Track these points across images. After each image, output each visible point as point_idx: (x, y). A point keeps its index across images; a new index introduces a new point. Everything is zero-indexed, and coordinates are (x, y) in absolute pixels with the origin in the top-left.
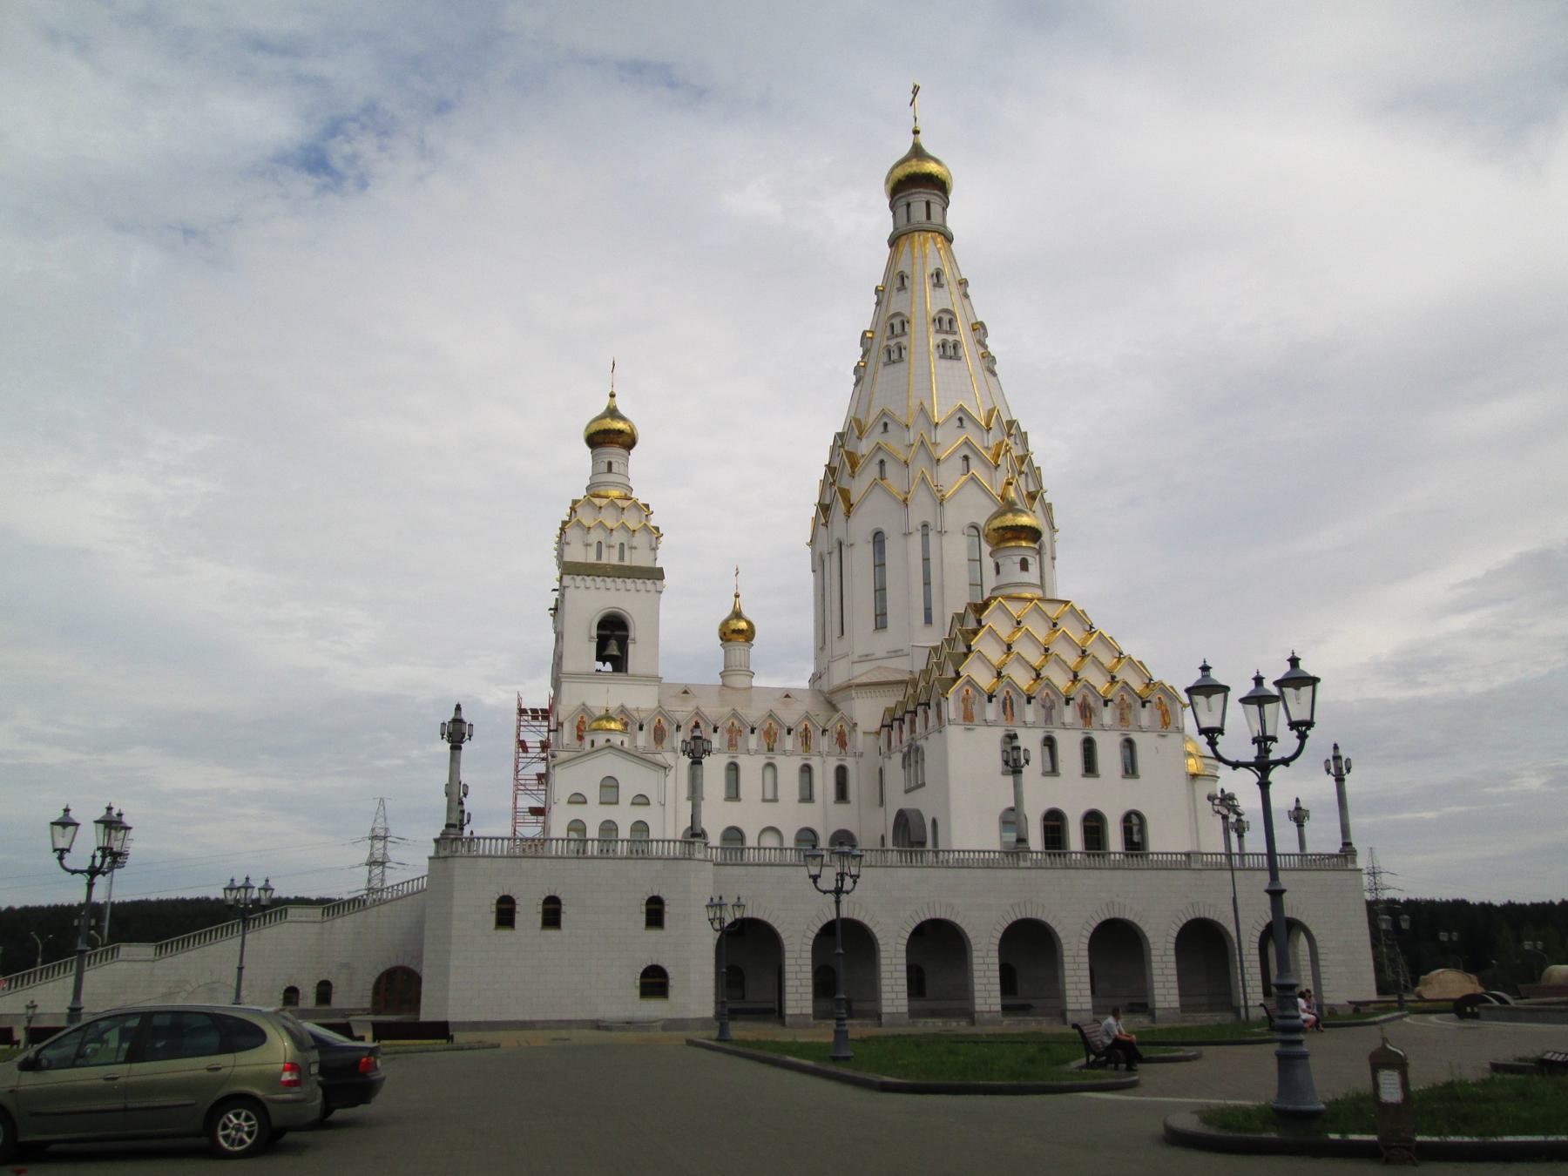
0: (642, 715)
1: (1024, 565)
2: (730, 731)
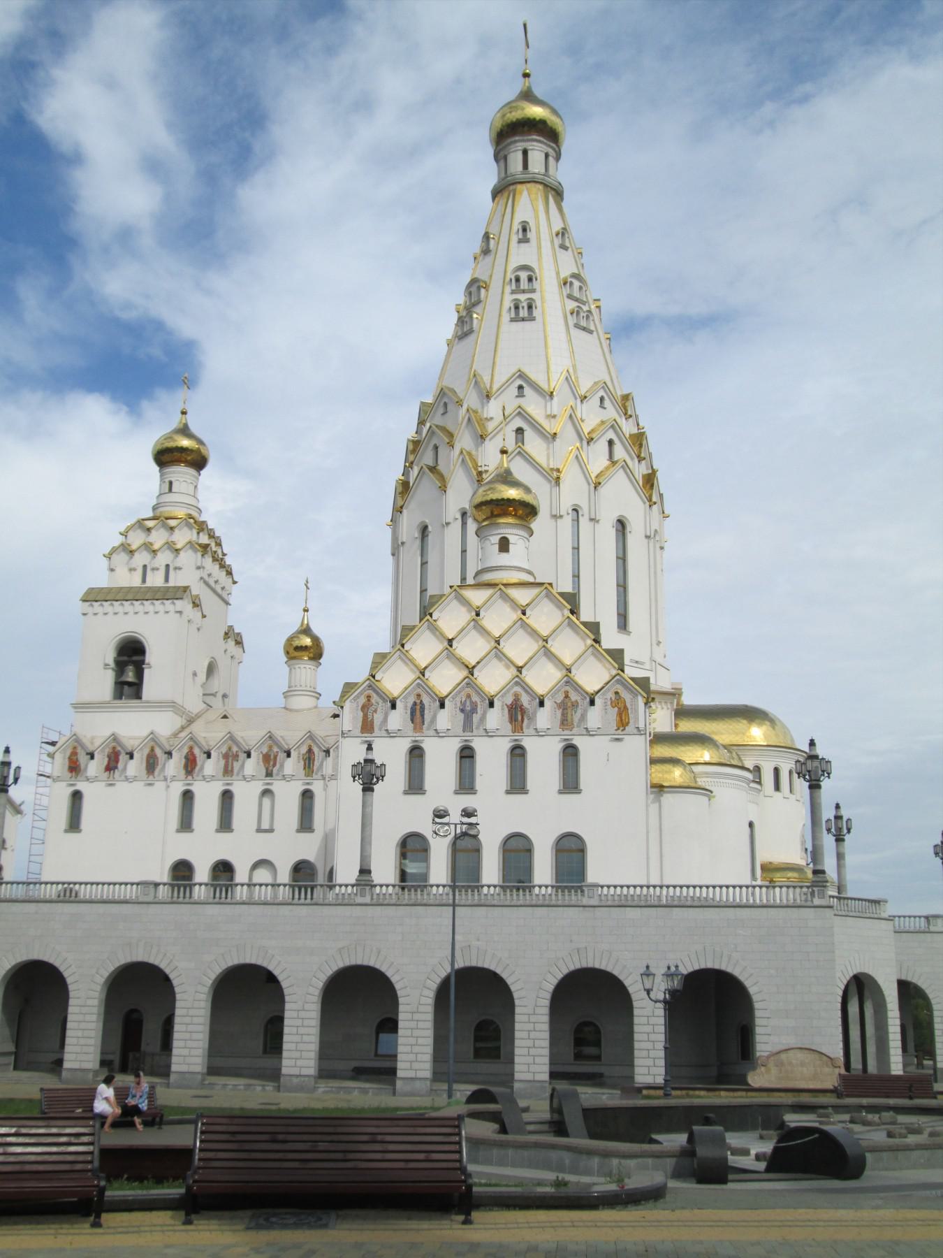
0: (132, 742)
1: (504, 545)
2: (226, 756)
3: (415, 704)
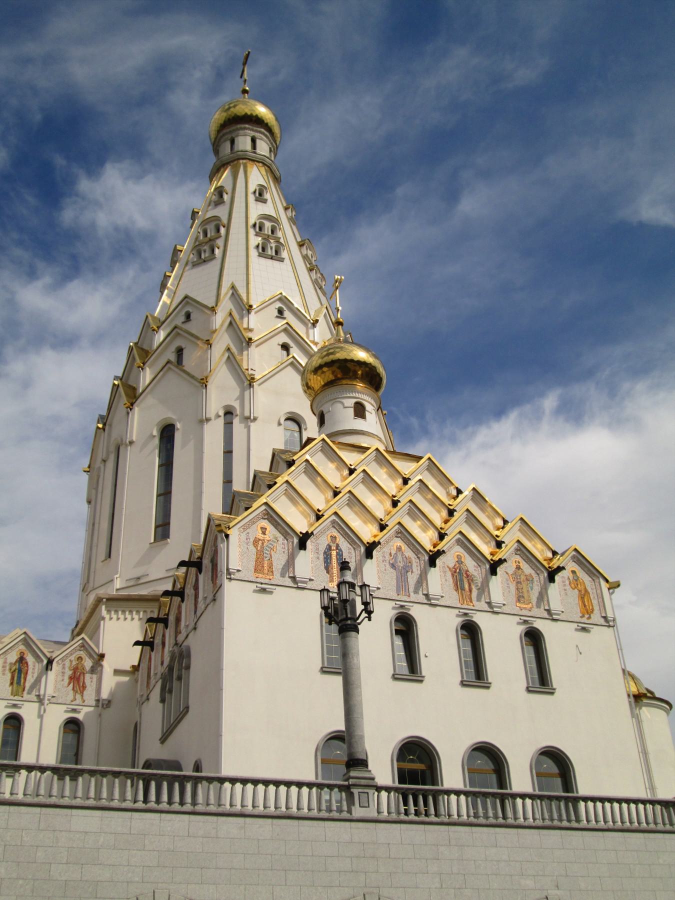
3: (329, 548)
